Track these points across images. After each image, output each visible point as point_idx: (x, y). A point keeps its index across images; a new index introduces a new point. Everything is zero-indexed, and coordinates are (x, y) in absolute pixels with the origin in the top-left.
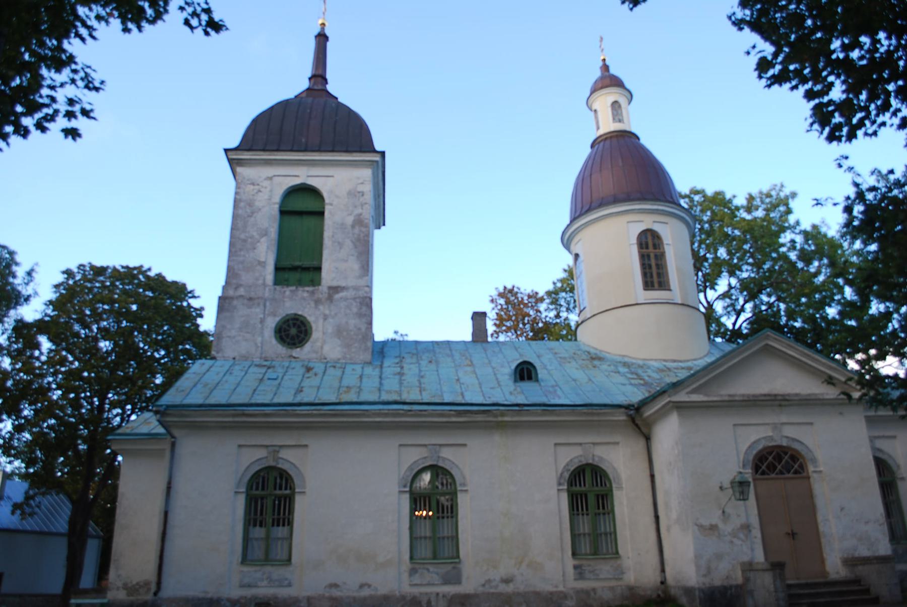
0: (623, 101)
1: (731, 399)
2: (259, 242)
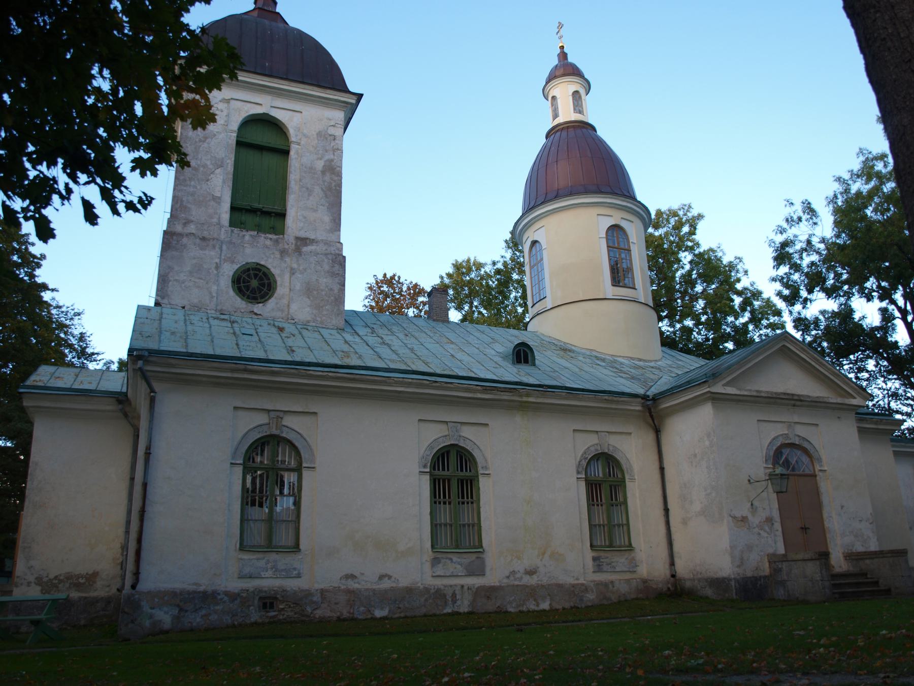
0: (582, 92)
1: (758, 394)
2: (213, 173)
